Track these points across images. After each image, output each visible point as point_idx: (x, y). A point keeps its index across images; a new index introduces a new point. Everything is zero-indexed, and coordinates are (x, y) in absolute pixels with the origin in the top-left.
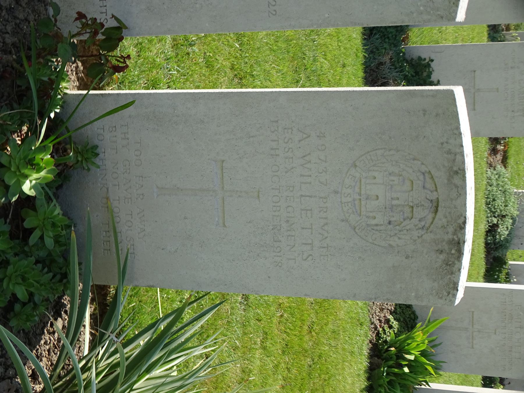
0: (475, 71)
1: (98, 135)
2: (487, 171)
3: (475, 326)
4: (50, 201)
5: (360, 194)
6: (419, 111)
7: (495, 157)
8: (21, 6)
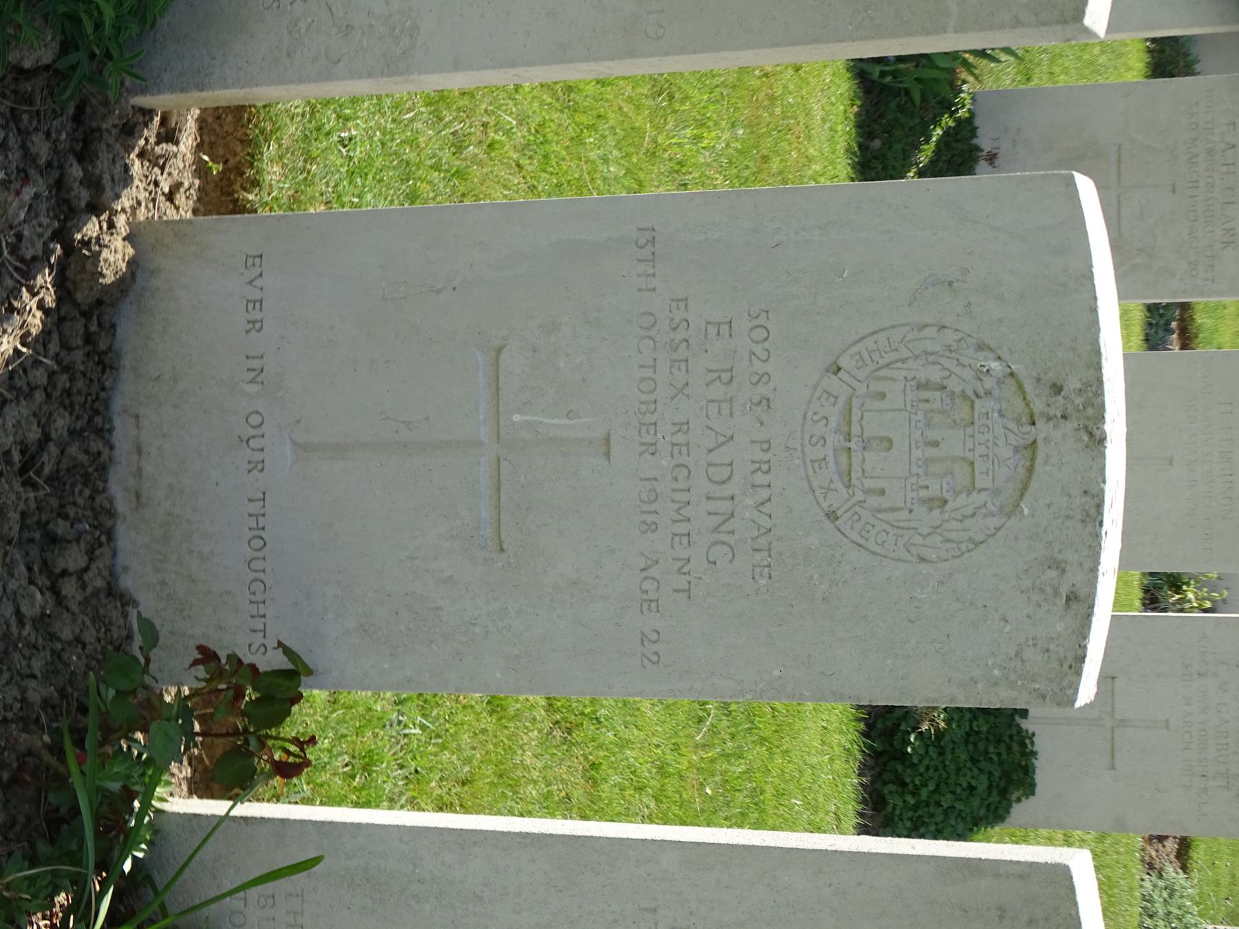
0: (1113, 678)
1: (232, 912)
2: (1143, 880)
4: (106, 435)
6: (989, 909)
7: (1160, 846)
8: (67, 609)
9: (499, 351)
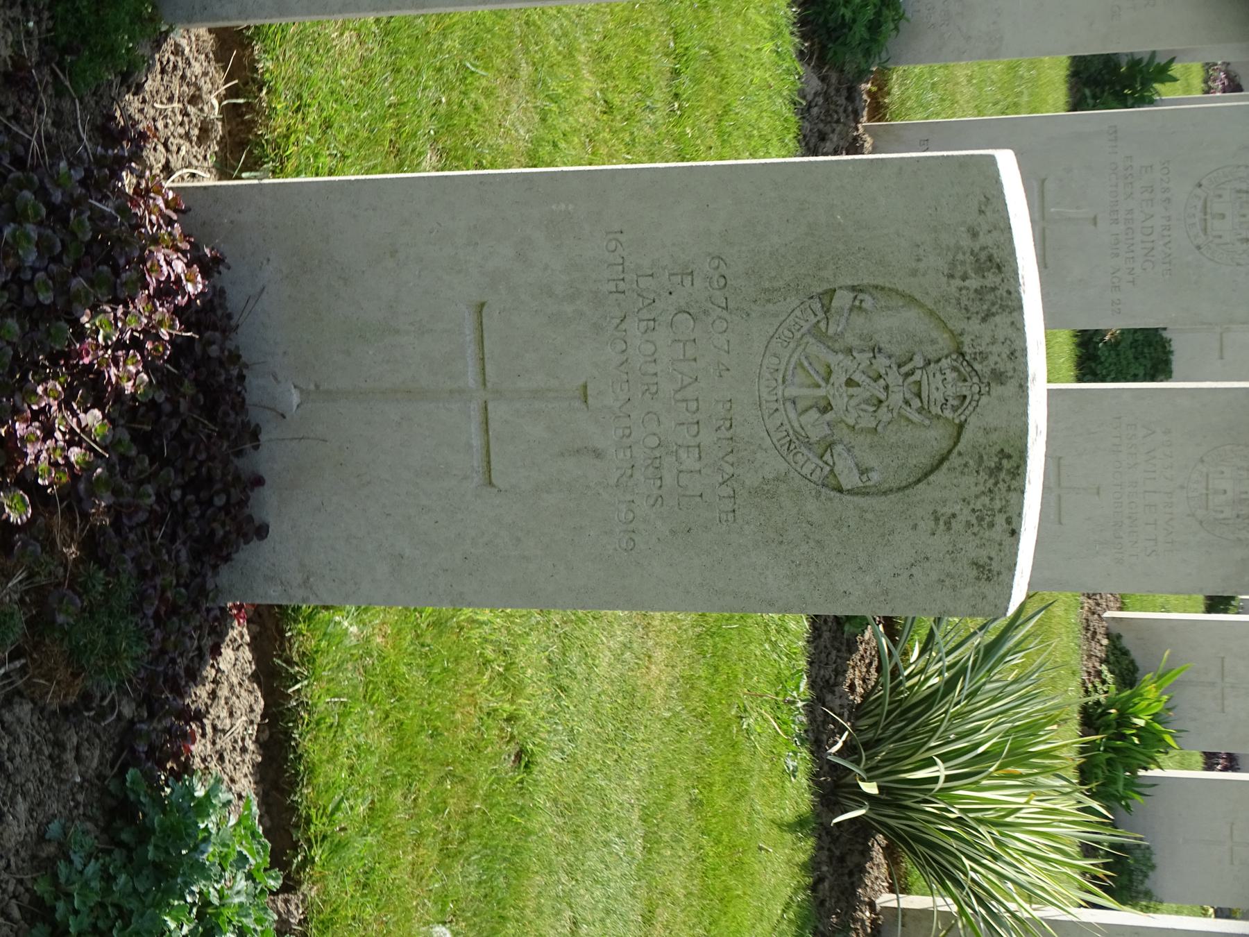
3: (1227, 680)
5: (1207, 489)
9: (1043, 181)
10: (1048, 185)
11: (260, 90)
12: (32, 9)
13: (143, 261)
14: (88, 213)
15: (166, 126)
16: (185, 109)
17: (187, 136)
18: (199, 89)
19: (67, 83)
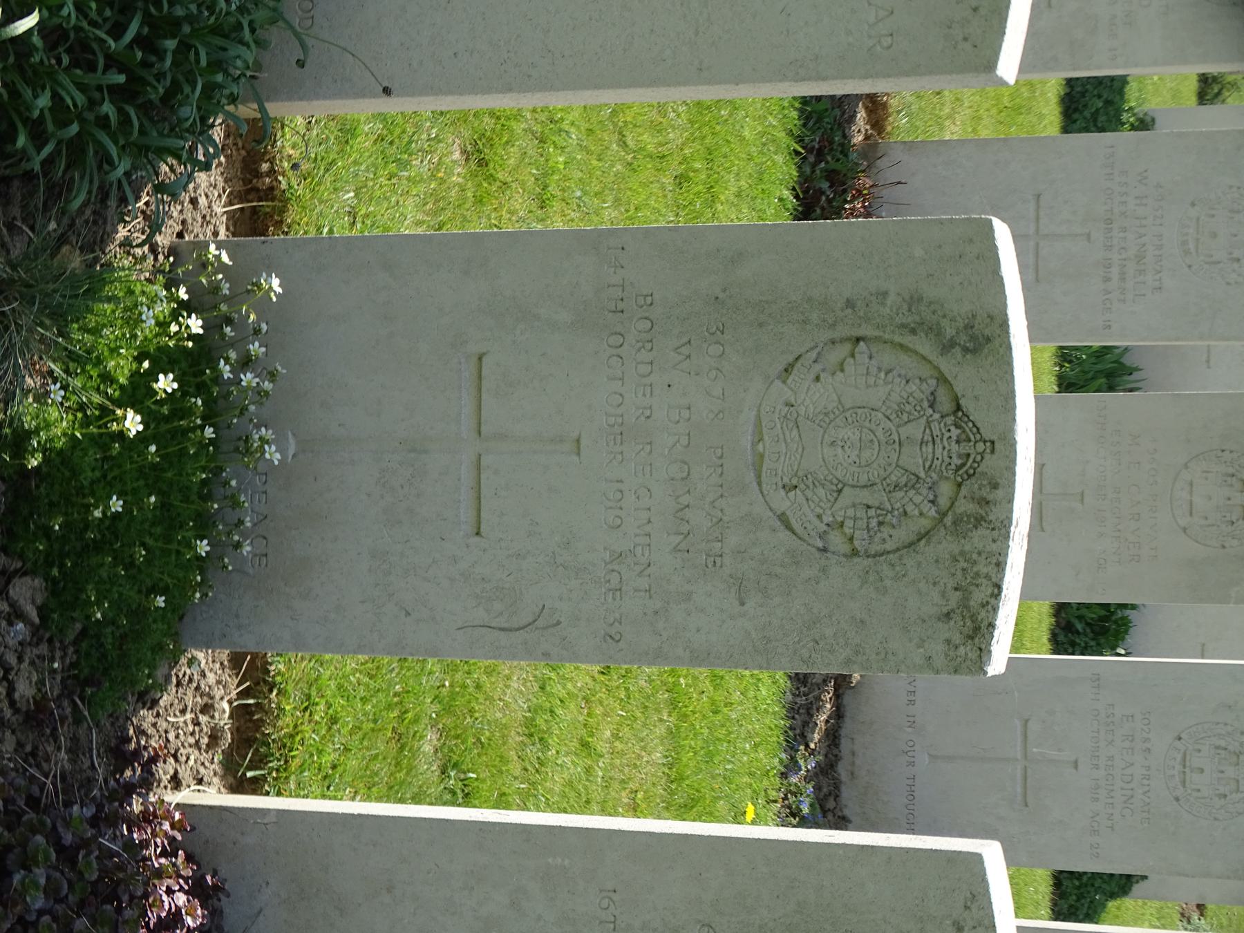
9: (1027, 721)
10: (1030, 724)
11: (271, 691)
12: (58, 645)
13: (146, 896)
14: (97, 853)
15: (177, 737)
16: (197, 718)
17: (197, 745)
18: (212, 698)
19: (86, 713)
